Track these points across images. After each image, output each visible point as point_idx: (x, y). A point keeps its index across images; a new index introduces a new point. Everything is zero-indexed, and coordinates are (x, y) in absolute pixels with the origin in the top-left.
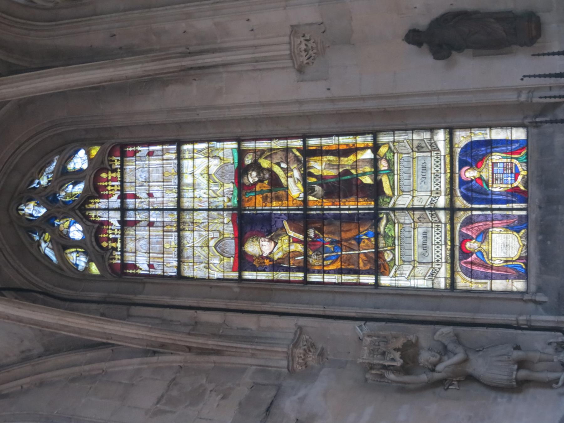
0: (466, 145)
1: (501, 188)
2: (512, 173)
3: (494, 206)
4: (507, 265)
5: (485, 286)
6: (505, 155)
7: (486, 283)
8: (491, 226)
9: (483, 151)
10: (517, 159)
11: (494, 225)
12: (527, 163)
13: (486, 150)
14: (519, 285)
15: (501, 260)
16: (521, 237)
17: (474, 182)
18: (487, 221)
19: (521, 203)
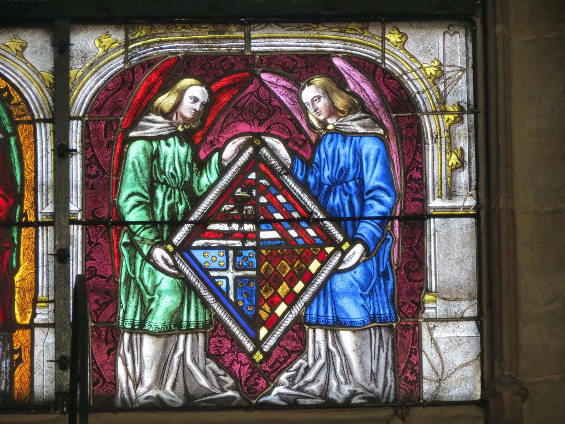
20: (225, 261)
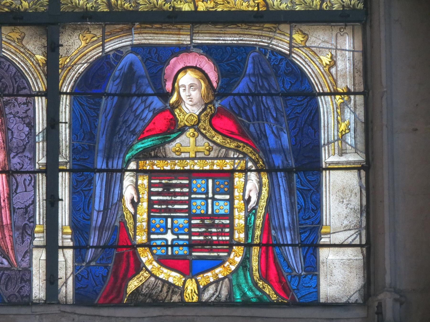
0: (300, 75)
1: (135, 204)
2: (192, 246)
3: (64, 180)
6: (259, 222)
9: (278, 137)
10: (245, 264)
12: (230, 303)
13: (282, 150)
17: (157, 103)
19: (76, 280)
20: (205, 209)
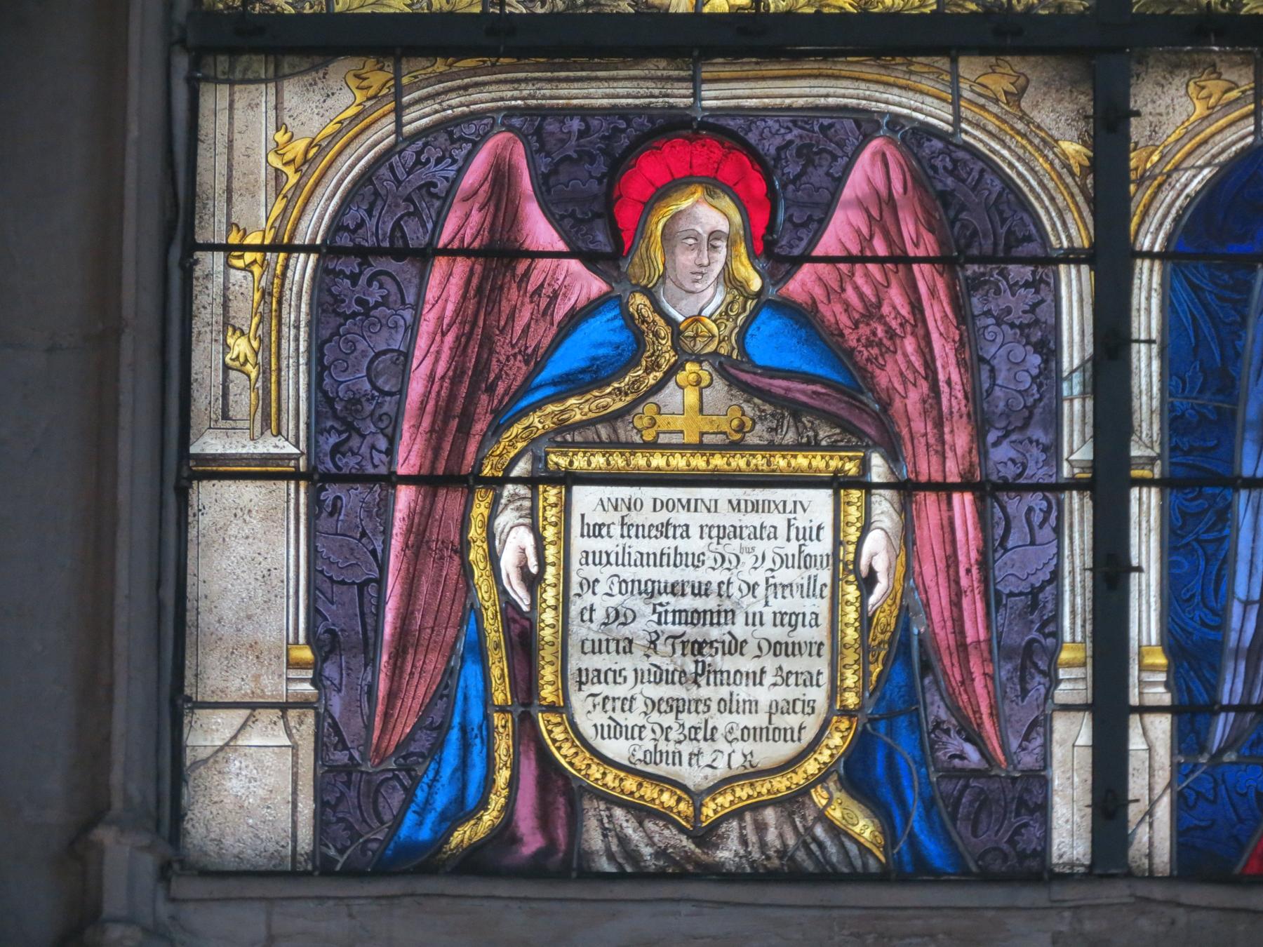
3: (1145, 511)
4: (479, 651)
5: (243, 401)
7: (269, 420)
8: (927, 469)
11: (929, 503)
14: (254, 779)
15: (532, 582)
16: (793, 802)
18: (980, 424)
